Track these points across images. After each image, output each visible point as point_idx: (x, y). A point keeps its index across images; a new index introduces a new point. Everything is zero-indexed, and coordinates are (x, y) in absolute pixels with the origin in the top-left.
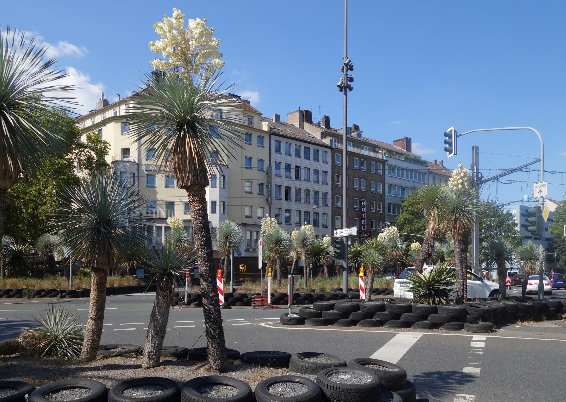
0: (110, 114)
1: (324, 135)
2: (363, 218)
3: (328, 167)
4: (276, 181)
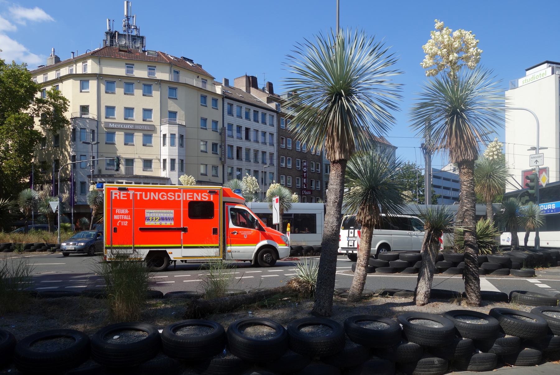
0: (64, 71)
1: (269, 100)
2: (304, 178)
3: (274, 130)
4: (229, 141)
